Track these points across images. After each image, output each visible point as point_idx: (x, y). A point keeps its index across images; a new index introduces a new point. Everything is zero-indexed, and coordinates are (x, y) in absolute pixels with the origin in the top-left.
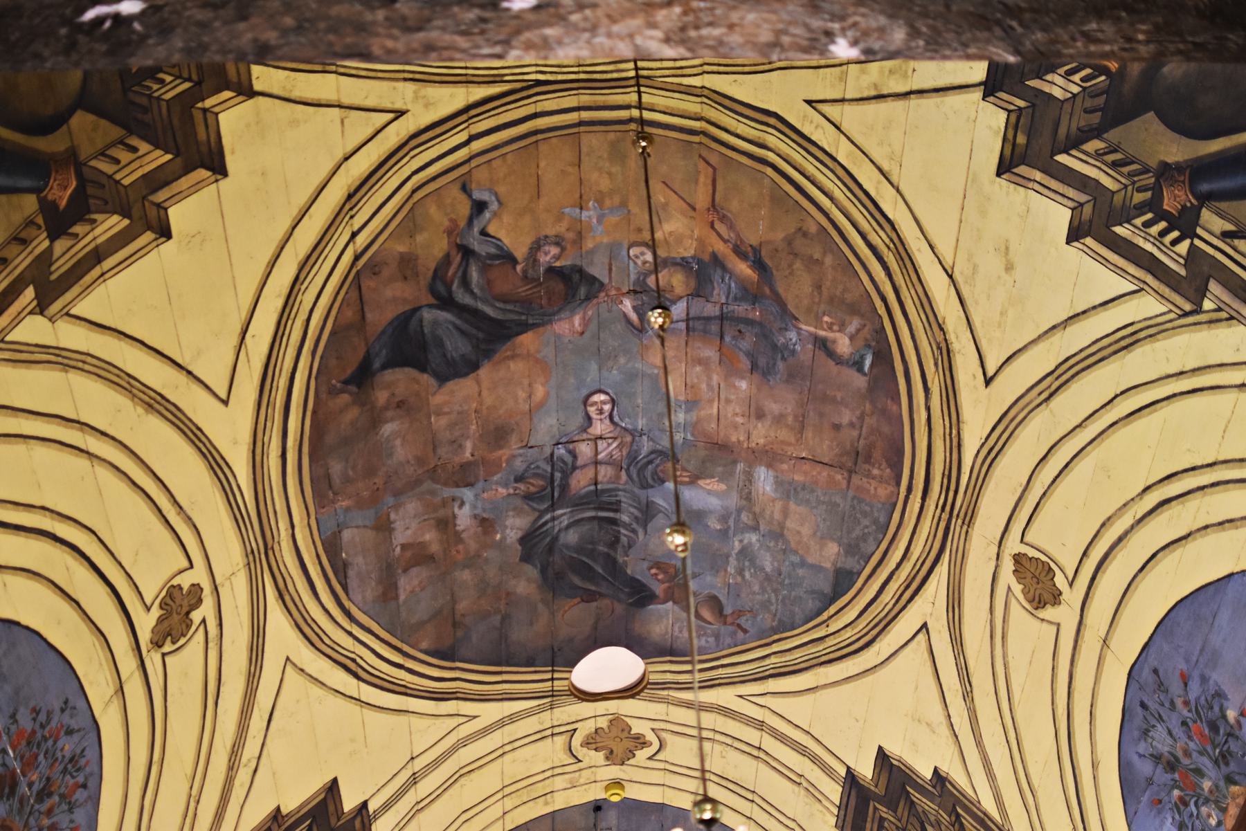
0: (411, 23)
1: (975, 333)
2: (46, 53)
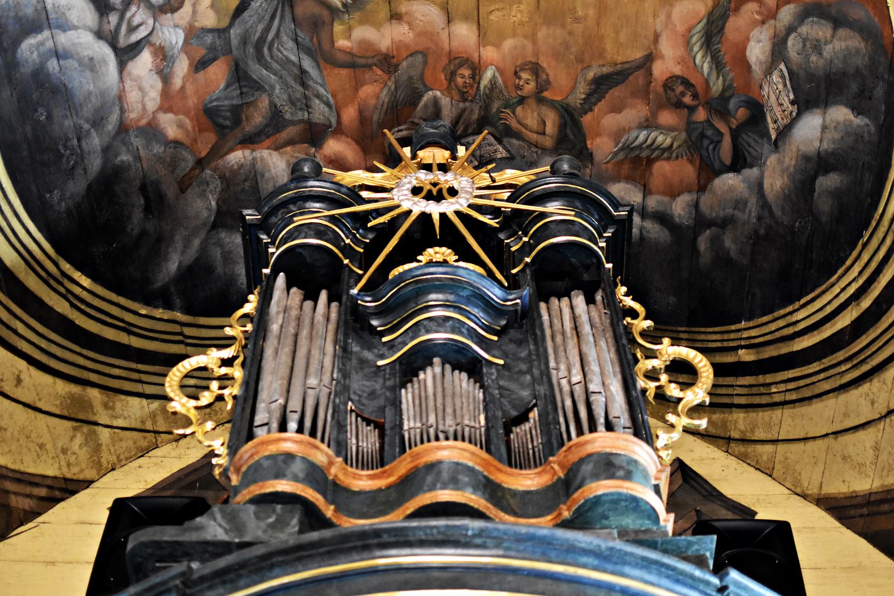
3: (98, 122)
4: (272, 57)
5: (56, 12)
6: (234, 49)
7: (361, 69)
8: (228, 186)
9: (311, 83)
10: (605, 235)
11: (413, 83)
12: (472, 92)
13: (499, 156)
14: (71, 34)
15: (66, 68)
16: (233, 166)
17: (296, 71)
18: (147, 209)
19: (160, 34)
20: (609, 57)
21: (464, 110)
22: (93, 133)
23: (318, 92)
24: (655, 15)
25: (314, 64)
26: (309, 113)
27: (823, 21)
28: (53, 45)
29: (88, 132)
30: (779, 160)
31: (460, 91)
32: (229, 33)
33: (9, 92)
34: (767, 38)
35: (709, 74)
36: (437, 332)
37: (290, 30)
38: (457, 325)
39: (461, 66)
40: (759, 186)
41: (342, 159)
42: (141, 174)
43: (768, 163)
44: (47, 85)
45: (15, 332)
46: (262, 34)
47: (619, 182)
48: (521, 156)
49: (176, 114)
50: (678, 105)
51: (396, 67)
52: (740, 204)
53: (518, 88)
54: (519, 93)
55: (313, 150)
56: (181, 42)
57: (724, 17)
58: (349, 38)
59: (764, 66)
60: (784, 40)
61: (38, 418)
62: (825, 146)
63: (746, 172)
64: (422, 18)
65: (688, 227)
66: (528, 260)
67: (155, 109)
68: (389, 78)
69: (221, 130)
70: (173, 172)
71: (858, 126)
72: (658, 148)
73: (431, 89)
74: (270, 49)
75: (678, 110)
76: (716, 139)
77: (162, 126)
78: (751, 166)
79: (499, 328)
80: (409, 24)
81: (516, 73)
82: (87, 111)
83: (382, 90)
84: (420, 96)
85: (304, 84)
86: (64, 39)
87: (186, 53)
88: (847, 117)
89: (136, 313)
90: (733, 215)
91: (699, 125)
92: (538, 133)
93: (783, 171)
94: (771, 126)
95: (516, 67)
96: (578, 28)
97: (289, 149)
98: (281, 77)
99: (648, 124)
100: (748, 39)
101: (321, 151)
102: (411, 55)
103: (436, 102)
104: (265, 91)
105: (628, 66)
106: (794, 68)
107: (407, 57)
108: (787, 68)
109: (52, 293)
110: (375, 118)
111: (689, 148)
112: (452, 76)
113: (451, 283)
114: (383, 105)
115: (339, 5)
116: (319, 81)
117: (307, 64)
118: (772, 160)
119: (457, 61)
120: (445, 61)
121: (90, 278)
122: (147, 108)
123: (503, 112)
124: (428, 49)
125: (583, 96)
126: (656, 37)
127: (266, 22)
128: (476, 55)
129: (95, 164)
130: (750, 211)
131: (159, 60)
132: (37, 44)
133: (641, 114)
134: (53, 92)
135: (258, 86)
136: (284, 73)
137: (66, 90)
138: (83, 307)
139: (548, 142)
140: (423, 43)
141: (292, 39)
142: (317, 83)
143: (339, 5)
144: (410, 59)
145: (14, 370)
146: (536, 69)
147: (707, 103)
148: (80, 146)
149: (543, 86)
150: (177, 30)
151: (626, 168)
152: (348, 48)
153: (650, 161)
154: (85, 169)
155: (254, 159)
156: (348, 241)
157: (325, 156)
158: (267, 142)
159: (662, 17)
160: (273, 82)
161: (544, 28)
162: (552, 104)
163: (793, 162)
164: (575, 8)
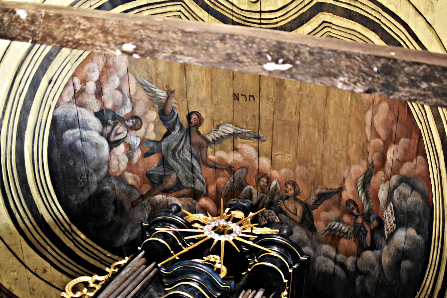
0: (166, 44)
1: (388, 21)
2: (307, 55)
3: (97, 170)
4: (179, 157)
5: (83, 122)
6: (163, 151)
7: (218, 170)
8: (154, 209)
9: (196, 172)
10: (294, 267)
11: (241, 180)
12: (267, 189)
13: (276, 221)
14: (89, 132)
15: (85, 145)
16: (157, 201)
17: (190, 165)
18: (116, 212)
19: (129, 139)
20: (325, 185)
21: (263, 197)
22: (94, 175)
23: (199, 176)
24: (344, 170)
25: (198, 164)
26: (194, 185)
27: (408, 186)
28: (80, 135)
29: (92, 174)
30: (388, 249)
31: (261, 188)
32: (161, 144)
33: (57, 150)
34: (386, 189)
35: (364, 202)
36: (183, 291)
37: (189, 147)
38: (195, 290)
39: (262, 177)
40: (379, 260)
41: (207, 208)
42: (115, 196)
43: (384, 249)
44: (75, 151)
45: (46, 250)
46: (176, 146)
47: (326, 244)
48: (286, 223)
49: (133, 173)
50: (351, 213)
51: (234, 172)
52: (372, 266)
53: (286, 191)
54: (287, 194)
55: (194, 201)
56: (138, 144)
57: (371, 176)
58: (214, 155)
59: (385, 202)
60: (393, 192)
61: (52, 289)
62: (406, 246)
63: (375, 251)
64: (247, 152)
65: (352, 272)
66: (249, 270)
67: (123, 170)
68: (231, 177)
69: (153, 185)
70: (129, 198)
71: (418, 240)
72: (342, 232)
73: (249, 185)
74: (179, 154)
75: (351, 216)
76: (365, 233)
77: (126, 177)
78: (377, 249)
79: (216, 297)
80: (241, 153)
81: (286, 185)
82: (93, 164)
83: (227, 181)
84: (244, 187)
85: (193, 172)
86: (85, 133)
87: (140, 149)
88: (414, 234)
89: (105, 255)
90: (369, 271)
91: (359, 225)
92: (294, 214)
93: (390, 254)
94: (386, 232)
95: (286, 182)
96: (313, 169)
97: (183, 199)
98: (183, 167)
99: (339, 220)
100: (379, 188)
101: (198, 203)
102: (241, 168)
103: (250, 191)
104: (175, 171)
105: (332, 191)
106: (396, 206)
107: (239, 169)
108: (393, 205)
109: (66, 238)
110: (223, 193)
111: (354, 234)
112: (258, 181)
113: (198, 271)
114: (227, 187)
115: (211, 140)
116: (200, 172)
117: (195, 163)
118: (385, 248)
119: (261, 174)
120: (256, 173)
121: (85, 235)
122: (120, 168)
123: (279, 201)
124: (249, 166)
125: (313, 201)
126: (344, 180)
127: (178, 142)
128: (269, 173)
129: (94, 188)
130: (376, 271)
131: (128, 149)
132: (73, 133)
133: (337, 214)
134: (78, 154)
135: (172, 169)
136: (184, 165)
137: (84, 155)
138: (80, 247)
139: (298, 219)
140: (247, 164)
141: (189, 151)
142: (199, 172)
143: (211, 140)
144: (241, 169)
145: (43, 266)
146: (294, 185)
147: (362, 215)
148: (87, 179)
149: (297, 193)
150: (137, 138)
151: (329, 238)
152: (213, 159)
153: (339, 238)
154: (89, 189)
155: (167, 200)
156: (180, 244)
157: (200, 205)
158: (174, 194)
159: (347, 171)
160: (179, 168)
161: (299, 166)
162: (300, 202)
163: (393, 251)
164: (312, 159)
